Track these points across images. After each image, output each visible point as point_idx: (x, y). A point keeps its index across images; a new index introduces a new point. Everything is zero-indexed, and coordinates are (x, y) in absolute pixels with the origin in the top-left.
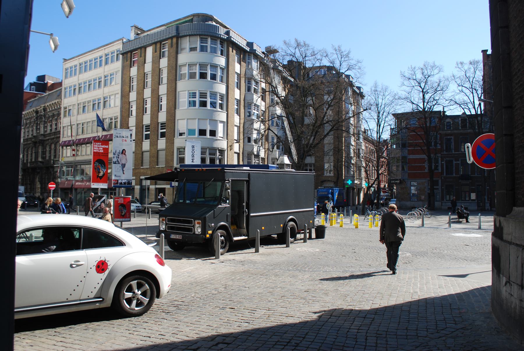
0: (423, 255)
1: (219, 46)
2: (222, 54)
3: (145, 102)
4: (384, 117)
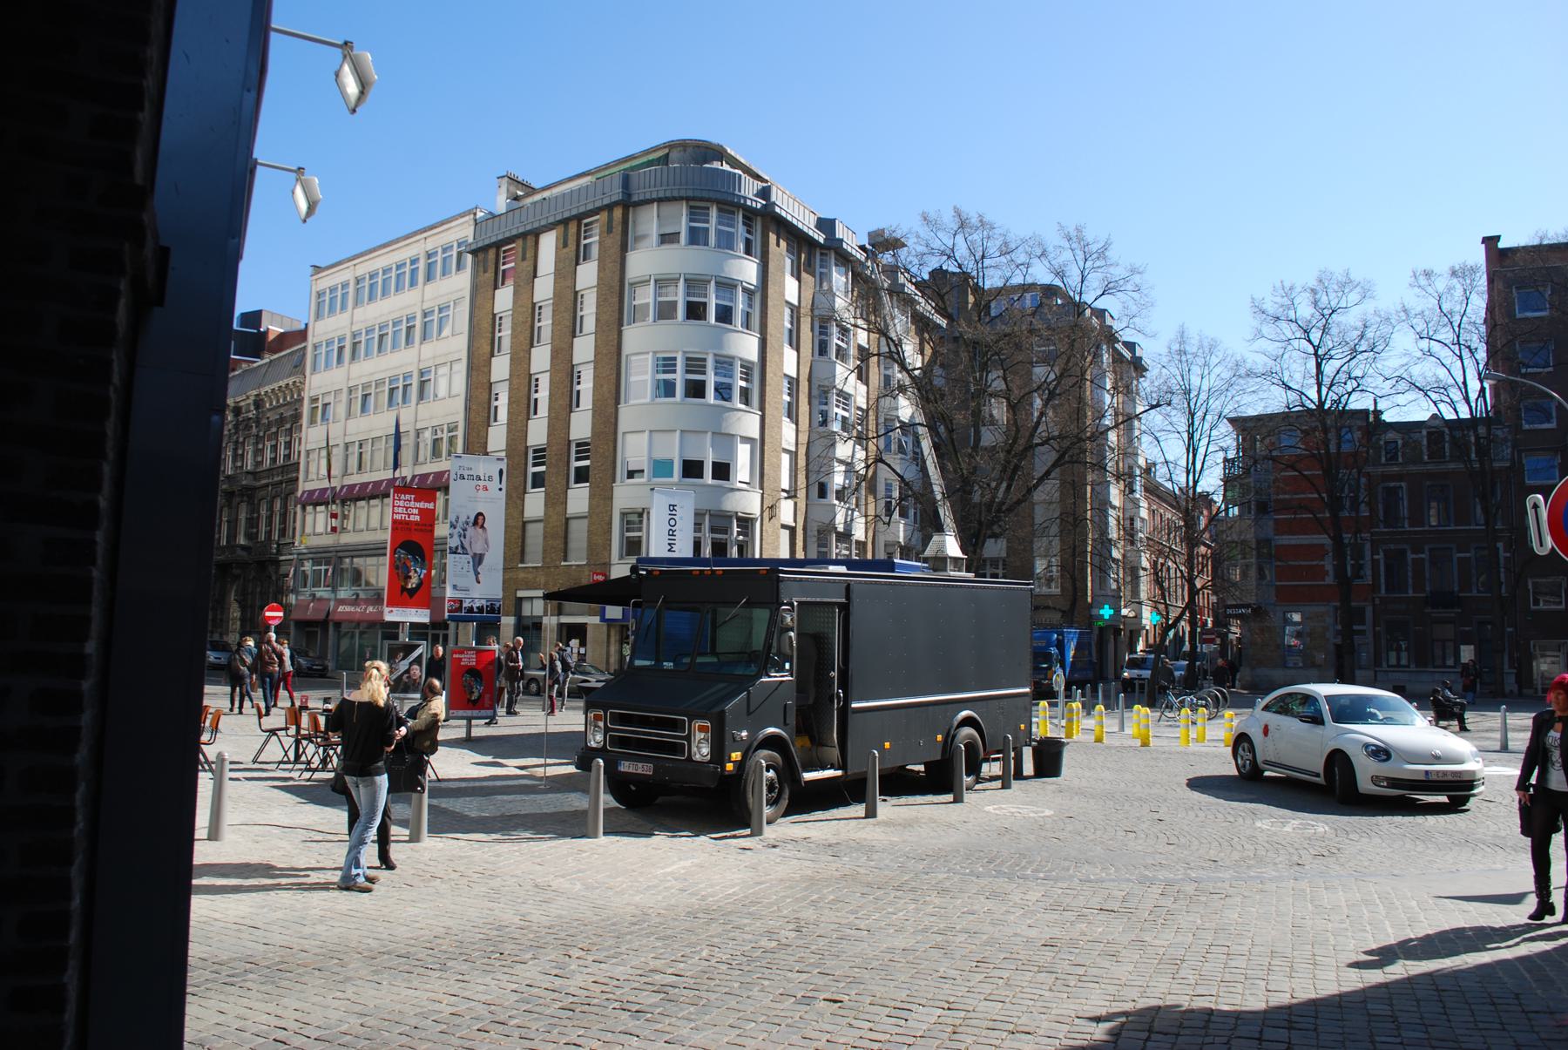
0: (1369, 831)
1: (741, 229)
2: (748, 251)
3: (533, 383)
4: (1207, 426)
